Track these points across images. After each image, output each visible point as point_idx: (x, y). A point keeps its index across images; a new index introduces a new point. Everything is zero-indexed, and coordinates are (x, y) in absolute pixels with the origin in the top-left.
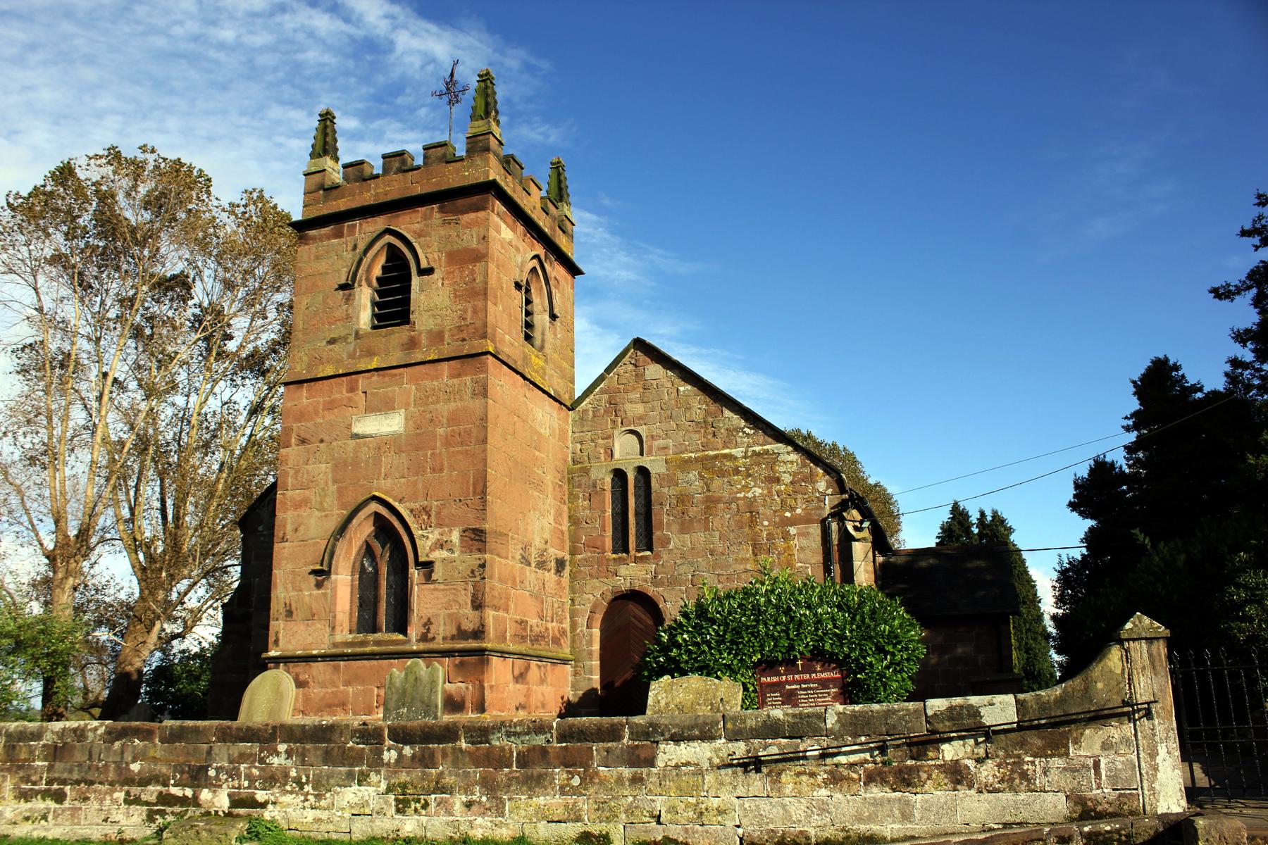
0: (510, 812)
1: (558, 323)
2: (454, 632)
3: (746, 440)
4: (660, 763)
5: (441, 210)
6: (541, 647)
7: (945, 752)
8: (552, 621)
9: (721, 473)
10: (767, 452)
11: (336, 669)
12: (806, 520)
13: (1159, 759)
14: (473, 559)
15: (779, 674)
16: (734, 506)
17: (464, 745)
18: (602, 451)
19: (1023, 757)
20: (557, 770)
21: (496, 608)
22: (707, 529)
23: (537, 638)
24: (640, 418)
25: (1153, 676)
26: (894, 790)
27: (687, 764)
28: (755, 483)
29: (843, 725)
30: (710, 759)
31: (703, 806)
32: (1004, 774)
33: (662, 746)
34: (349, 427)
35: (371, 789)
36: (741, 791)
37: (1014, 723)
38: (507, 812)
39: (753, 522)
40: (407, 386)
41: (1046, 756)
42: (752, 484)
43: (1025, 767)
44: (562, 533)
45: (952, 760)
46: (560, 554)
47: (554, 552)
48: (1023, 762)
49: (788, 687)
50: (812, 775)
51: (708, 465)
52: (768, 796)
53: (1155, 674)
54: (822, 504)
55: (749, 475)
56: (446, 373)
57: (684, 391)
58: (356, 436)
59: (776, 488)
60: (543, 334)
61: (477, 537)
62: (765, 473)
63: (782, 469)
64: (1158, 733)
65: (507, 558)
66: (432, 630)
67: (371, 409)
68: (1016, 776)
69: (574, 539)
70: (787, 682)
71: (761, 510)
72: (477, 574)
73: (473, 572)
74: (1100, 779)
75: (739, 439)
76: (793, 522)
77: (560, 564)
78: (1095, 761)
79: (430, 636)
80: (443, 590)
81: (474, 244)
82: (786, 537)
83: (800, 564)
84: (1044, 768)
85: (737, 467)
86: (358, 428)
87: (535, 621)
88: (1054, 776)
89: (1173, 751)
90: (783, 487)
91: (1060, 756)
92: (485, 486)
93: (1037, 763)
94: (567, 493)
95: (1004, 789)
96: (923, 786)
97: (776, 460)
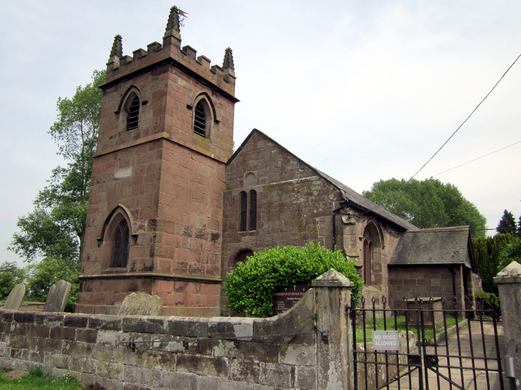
0: (46, 361)
1: (221, 124)
2: (143, 267)
3: (299, 175)
4: (98, 341)
5: (152, 74)
6: (197, 275)
7: (215, 351)
8: (207, 263)
9: (287, 192)
10: (307, 181)
11: (102, 283)
12: (324, 214)
13: (329, 372)
14: (151, 234)
15: (284, 292)
16: (291, 208)
17: (35, 324)
18: (239, 183)
19: (254, 360)
20: (63, 340)
21: (161, 256)
22: (279, 219)
23: (195, 271)
24: (255, 167)
25: (331, 314)
26: (190, 371)
27: (107, 343)
28: (301, 196)
29: (170, 329)
30: (116, 341)
31: (111, 367)
32: (243, 369)
33: (99, 332)
34: (113, 175)
35: (5, 343)
36: (126, 362)
37: (251, 337)
38: (44, 361)
39: (300, 215)
40: (133, 156)
41: (266, 361)
42: (300, 196)
43: (254, 367)
44: (218, 222)
45: (218, 357)
46: (215, 232)
47: (210, 231)
48: (252, 363)
49: (288, 299)
50: (155, 356)
51: (282, 188)
52: (136, 366)
53: (332, 313)
54: (331, 206)
55: (298, 192)
56: (148, 148)
57: (274, 153)
58: (116, 179)
59: (310, 198)
60: (210, 130)
61: (153, 223)
62: (305, 191)
63: (314, 189)
64: (330, 354)
65: (173, 233)
66: (135, 267)
67: (121, 167)
68: (249, 372)
69: (225, 225)
70: (290, 297)
71: (304, 209)
72: (153, 240)
73: (151, 239)
74: (294, 381)
75: (296, 175)
76: (318, 215)
77: (215, 237)
78: (292, 368)
79: (134, 269)
80: (140, 248)
81: (163, 89)
82: (315, 223)
83: (320, 237)
84: (264, 369)
85: (294, 188)
86: (117, 176)
87: (193, 263)
88: (269, 375)
89: (338, 368)
90: (314, 198)
91: (273, 362)
92: (158, 200)
93: (260, 365)
94: (222, 203)
95: (242, 379)
96: (203, 371)
97: (311, 185)
